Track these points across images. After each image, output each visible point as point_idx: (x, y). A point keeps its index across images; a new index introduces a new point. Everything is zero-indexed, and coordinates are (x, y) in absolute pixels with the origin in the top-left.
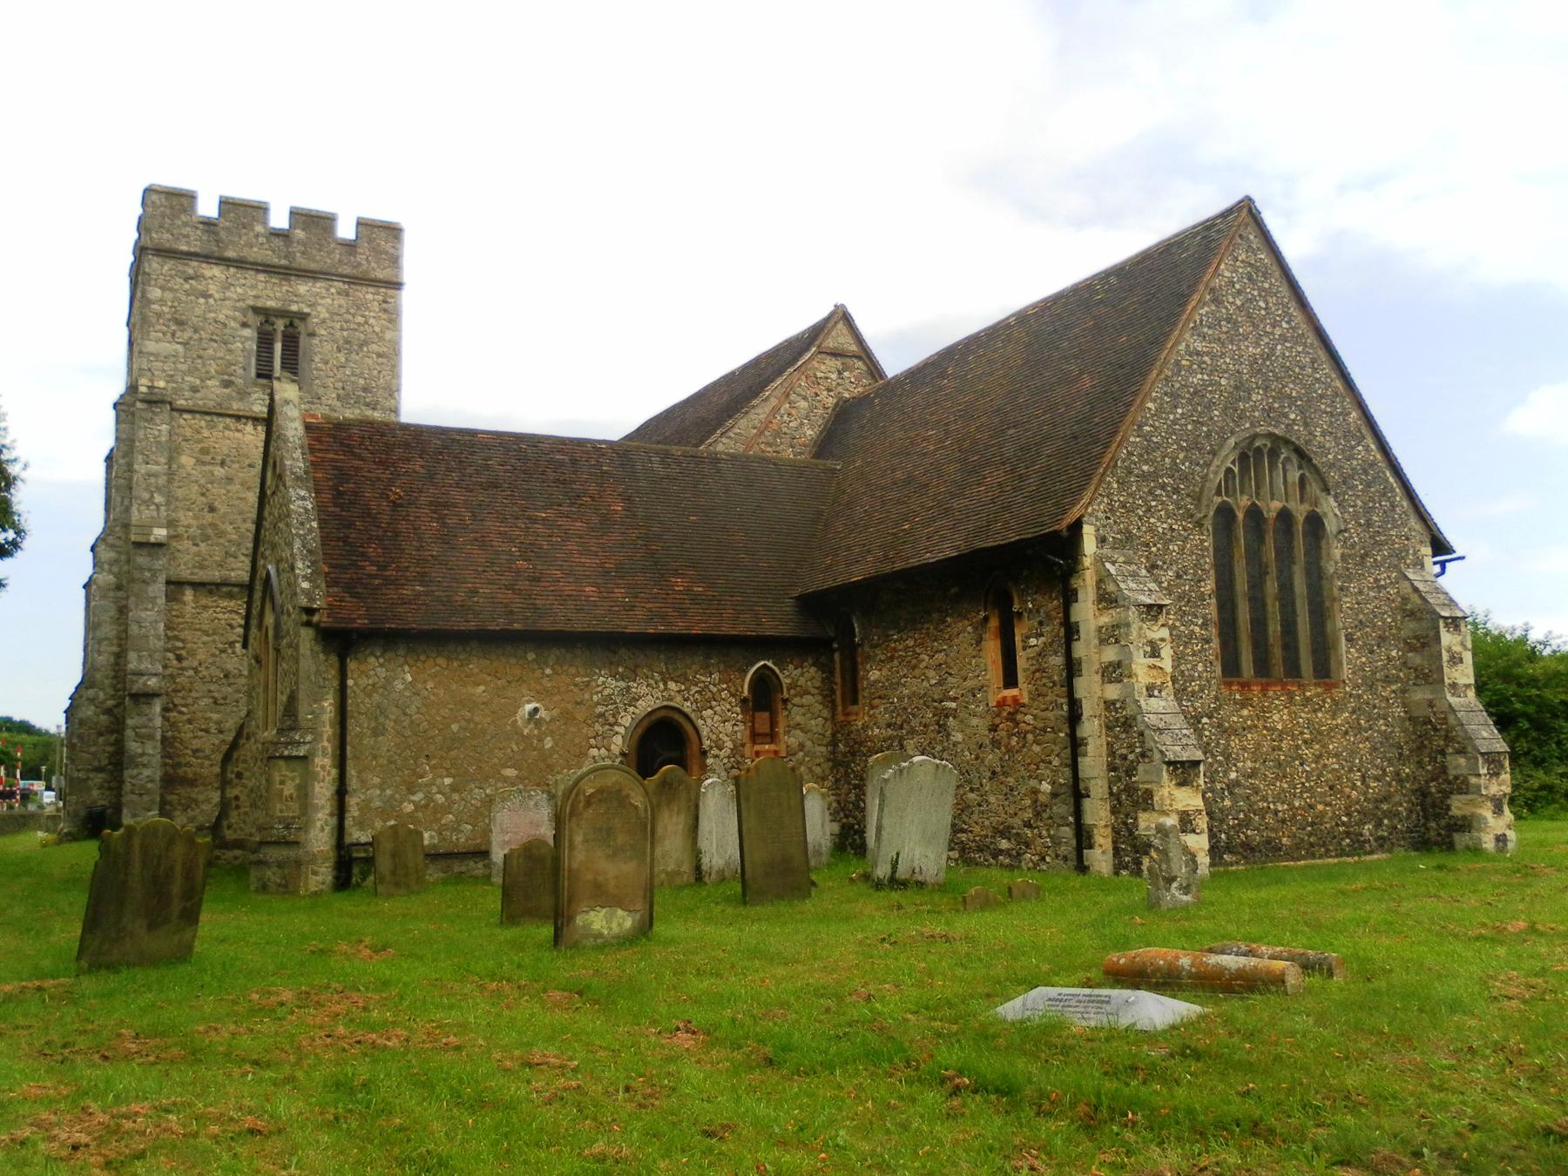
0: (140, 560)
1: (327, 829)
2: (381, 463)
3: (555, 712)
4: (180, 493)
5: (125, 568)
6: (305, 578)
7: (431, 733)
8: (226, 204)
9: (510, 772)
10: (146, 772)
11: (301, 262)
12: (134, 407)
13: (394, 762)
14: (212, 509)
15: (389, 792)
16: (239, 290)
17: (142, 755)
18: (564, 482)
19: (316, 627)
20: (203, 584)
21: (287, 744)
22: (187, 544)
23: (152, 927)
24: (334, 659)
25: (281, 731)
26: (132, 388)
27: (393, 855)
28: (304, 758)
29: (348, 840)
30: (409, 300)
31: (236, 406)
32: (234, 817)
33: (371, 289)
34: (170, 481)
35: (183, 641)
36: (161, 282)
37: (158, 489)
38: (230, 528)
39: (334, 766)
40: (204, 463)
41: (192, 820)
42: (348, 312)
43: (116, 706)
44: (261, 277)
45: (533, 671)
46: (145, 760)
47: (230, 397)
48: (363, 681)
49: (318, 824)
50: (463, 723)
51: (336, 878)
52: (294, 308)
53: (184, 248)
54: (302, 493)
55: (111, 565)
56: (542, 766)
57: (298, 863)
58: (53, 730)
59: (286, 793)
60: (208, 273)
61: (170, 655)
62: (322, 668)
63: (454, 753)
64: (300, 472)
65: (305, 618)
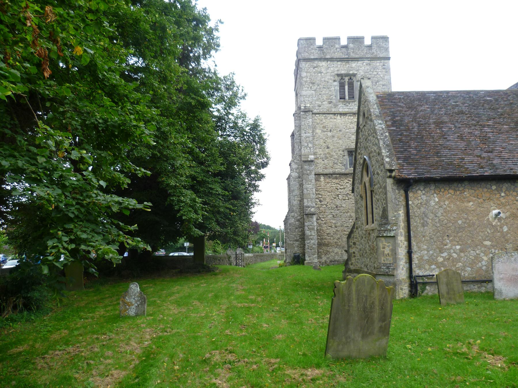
0: (305, 167)
1: (405, 269)
2: (409, 108)
3: (508, 214)
4: (317, 143)
5: (301, 170)
6: (387, 157)
7: (448, 225)
8: (326, 40)
9: (488, 243)
10: (312, 242)
11: (353, 55)
12: (301, 113)
13: (433, 239)
14: (328, 148)
15: (431, 252)
16: (332, 69)
17: (311, 235)
18: (493, 109)
19: (394, 178)
20: (326, 174)
21: (387, 230)
22: (320, 160)
23: (364, 336)
24: (402, 192)
25: (381, 225)
26: (299, 108)
27: (447, 284)
28: (394, 237)
29: (414, 274)
30: (392, 63)
31: (334, 110)
32: (353, 260)
33: (378, 61)
34: (313, 139)
35: (321, 195)
36: (306, 70)
37: (310, 142)
38: (334, 154)
39: (406, 241)
40: (324, 132)
41: (328, 258)
42: (370, 71)
43: (301, 218)
44: (339, 63)
45: (496, 194)
46: (311, 237)
47: (331, 107)
48: (416, 202)
49: (401, 267)
50: (464, 220)
51: (410, 291)
52: (351, 72)
53: (312, 57)
54: (380, 122)
55: (296, 170)
56: (503, 240)
57: (395, 284)
58: (277, 228)
59: (386, 252)
60: (321, 65)
61: (317, 200)
62: (397, 196)
63: (460, 234)
64: (378, 114)
65: (388, 174)
